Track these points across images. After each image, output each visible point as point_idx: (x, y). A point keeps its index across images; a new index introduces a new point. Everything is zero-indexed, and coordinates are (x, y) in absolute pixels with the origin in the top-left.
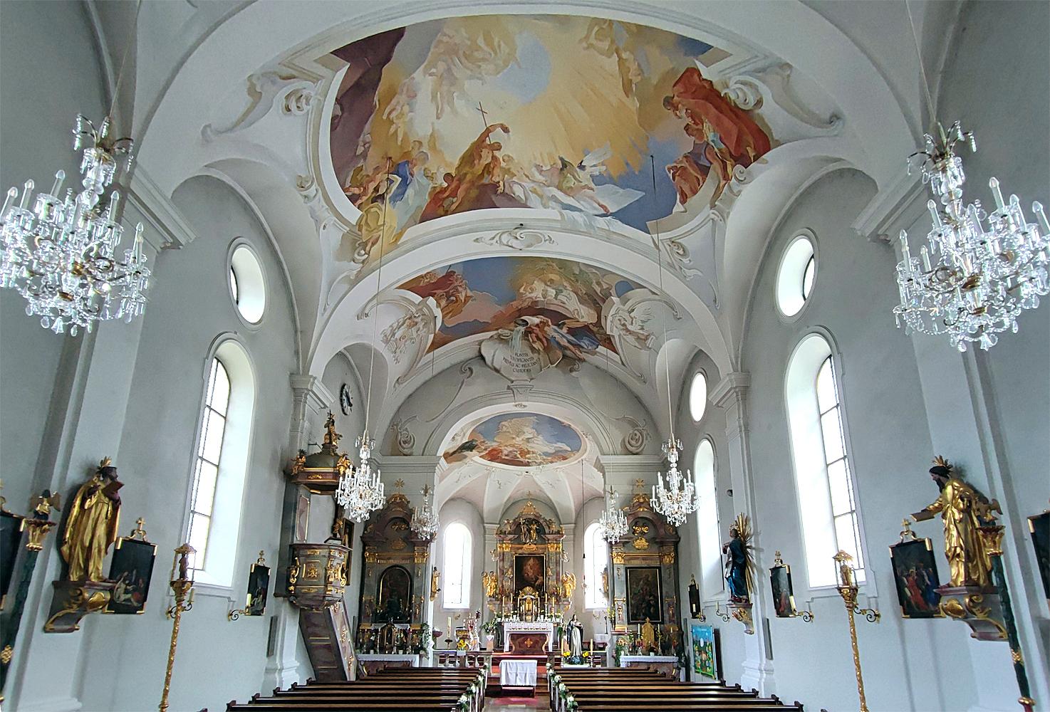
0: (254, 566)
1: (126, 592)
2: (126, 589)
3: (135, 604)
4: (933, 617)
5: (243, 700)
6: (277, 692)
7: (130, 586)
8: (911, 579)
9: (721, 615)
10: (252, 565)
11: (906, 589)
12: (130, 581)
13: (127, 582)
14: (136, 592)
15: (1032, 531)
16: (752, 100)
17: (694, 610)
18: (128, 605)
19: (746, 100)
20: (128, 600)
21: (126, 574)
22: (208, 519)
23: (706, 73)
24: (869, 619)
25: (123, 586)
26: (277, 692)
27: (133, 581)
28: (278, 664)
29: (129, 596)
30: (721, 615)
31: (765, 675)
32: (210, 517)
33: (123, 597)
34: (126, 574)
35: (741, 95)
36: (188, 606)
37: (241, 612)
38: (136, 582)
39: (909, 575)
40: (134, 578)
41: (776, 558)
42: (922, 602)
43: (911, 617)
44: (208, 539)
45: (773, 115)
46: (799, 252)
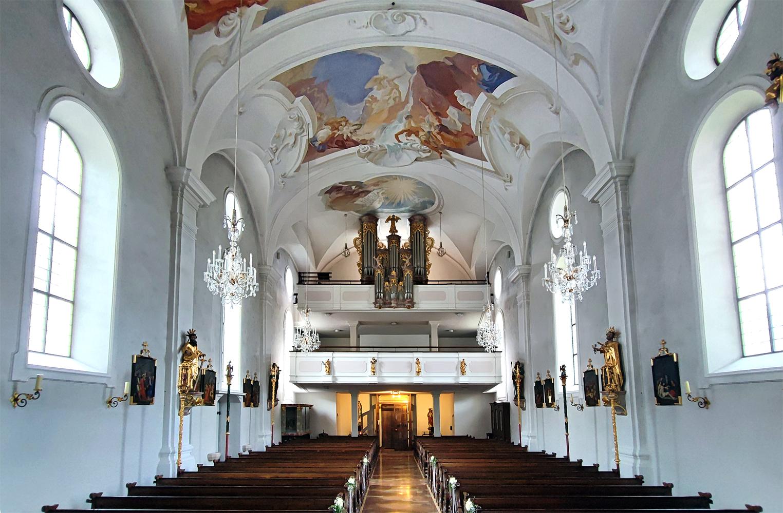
0: (135, 356)
1: (665, 391)
2: (664, 389)
3: (674, 398)
4: (674, 405)
5: (115, 488)
6: (181, 473)
7: (666, 386)
8: (142, 379)
9: (576, 405)
10: (133, 356)
11: (138, 386)
12: (665, 383)
13: (664, 384)
14: (672, 390)
15: (652, 365)
16: (223, 29)
17: (550, 402)
18: (668, 400)
19: (224, 24)
20: (668, 396)
21: (662, 379)
22: (71, 305)
23: (256, 8)
24: (701, 406)
25: (662, 387)
26: (181, 473)
27: (667, 382)
28: (171, 449)
29: (667, 393)
30: (576, 405)
31: (530, 439)
32: (73, 303)
33: (664, 394)
34: (662, 379)
35: (230, 22)
36: (35, 394)
37: (119, 399)
38: (670, 384)
39: (142, 377)
40: (667, 381)
41: (547, 374)
42: (144, 395)
43: (661, 405)
44: (72, 325)
45: (209, 39)
46: (559, 202)
